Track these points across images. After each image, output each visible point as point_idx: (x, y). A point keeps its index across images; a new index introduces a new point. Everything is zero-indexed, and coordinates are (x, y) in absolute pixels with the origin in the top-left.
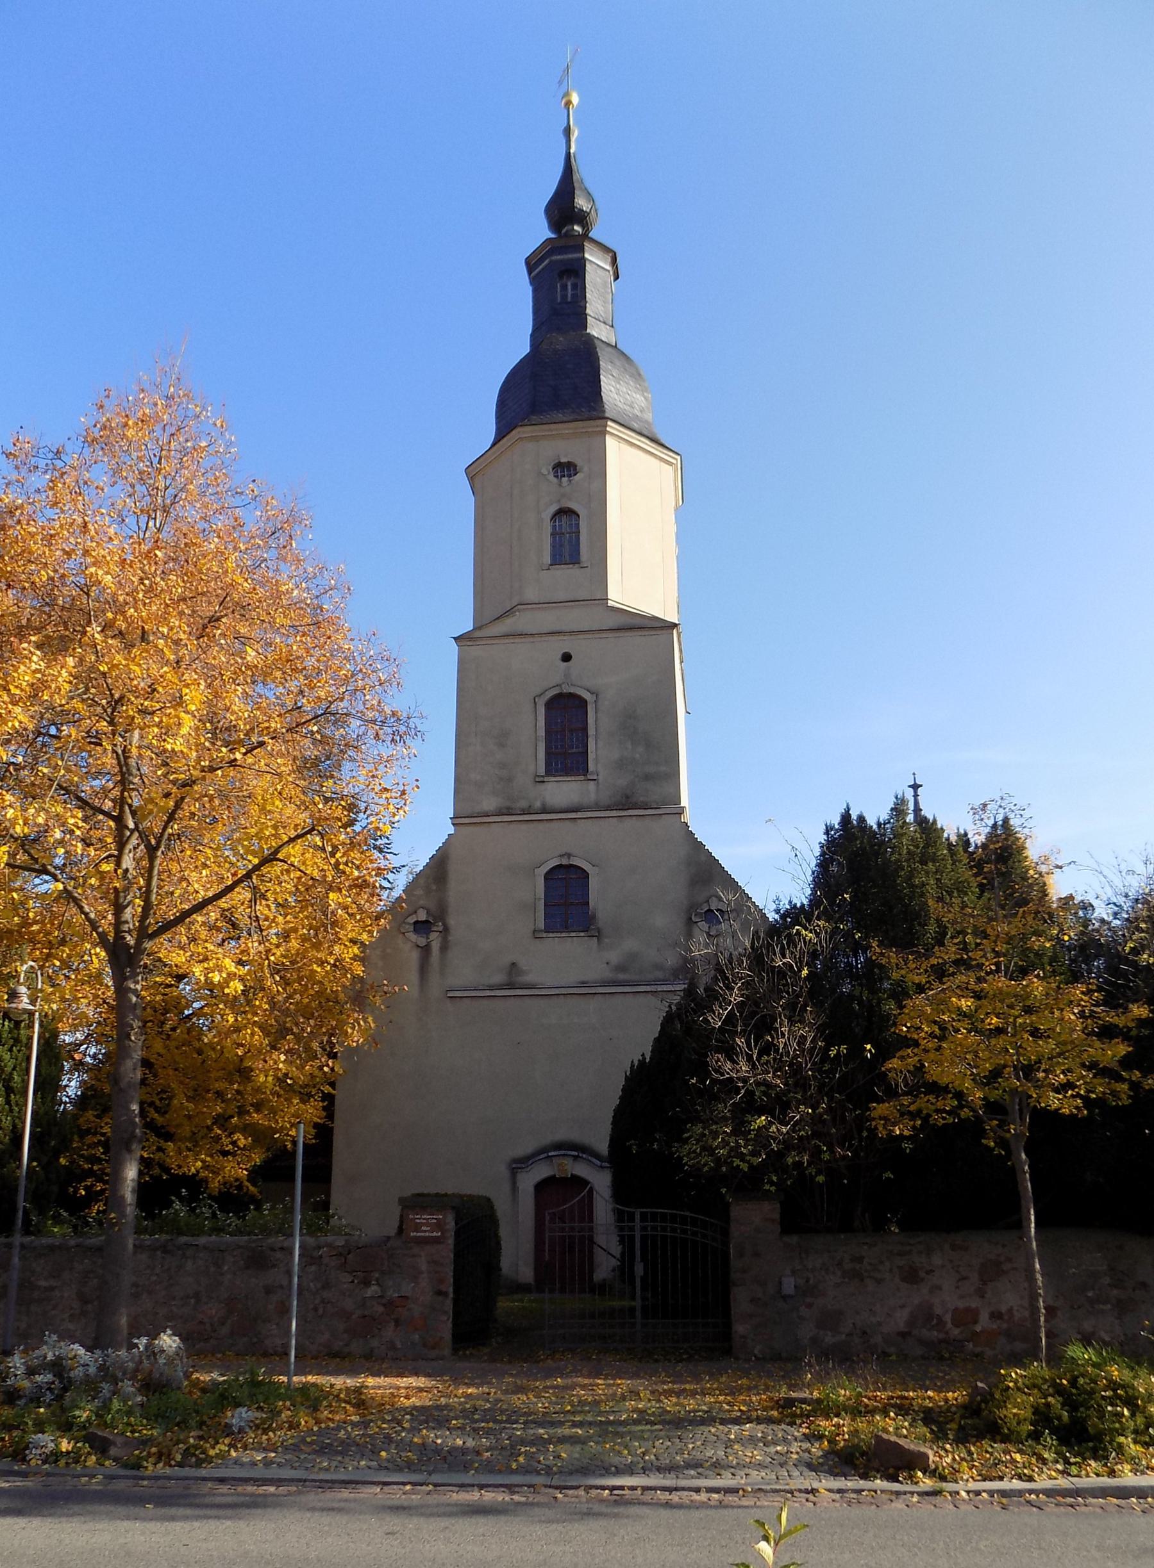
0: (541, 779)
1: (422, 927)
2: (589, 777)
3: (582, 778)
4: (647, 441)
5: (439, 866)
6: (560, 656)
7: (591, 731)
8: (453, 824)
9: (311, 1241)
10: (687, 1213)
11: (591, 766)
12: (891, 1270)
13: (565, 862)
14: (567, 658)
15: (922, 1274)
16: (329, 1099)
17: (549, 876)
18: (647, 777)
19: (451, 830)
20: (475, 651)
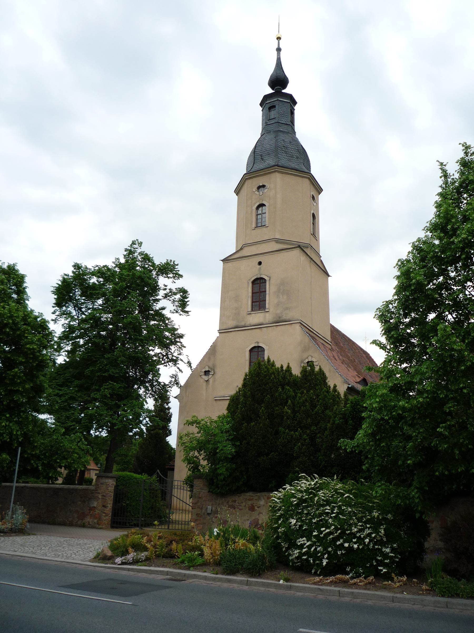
0: (249, 313)
1: (207, 373)
2: (267, 310)
3: (263, 311)
4: (295, 171)
5: (213, 350)
6: (257, 263)
7: (267, 292)
8: (219, 333)
9: (14, 468)
10: (80, 487)
11: (267, 306)
12: (245, 506)
13: (256, 345)
14: (260, 263)
15: (256, 508)
16: (270, 277)
17: (251, 350)
18: (287, 309)
19: (218, 335)
20: (229, 265)
